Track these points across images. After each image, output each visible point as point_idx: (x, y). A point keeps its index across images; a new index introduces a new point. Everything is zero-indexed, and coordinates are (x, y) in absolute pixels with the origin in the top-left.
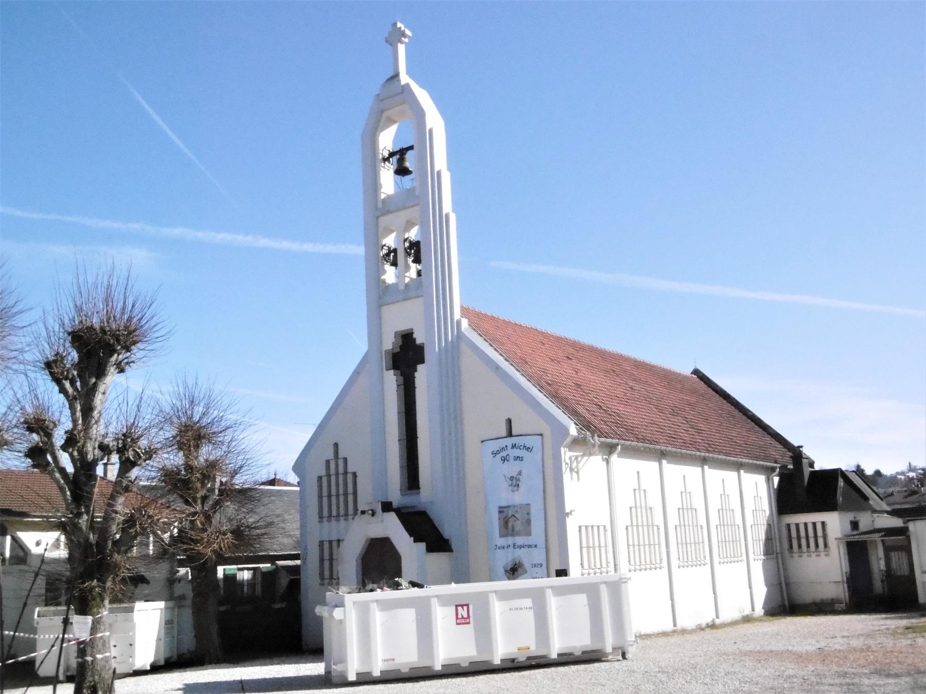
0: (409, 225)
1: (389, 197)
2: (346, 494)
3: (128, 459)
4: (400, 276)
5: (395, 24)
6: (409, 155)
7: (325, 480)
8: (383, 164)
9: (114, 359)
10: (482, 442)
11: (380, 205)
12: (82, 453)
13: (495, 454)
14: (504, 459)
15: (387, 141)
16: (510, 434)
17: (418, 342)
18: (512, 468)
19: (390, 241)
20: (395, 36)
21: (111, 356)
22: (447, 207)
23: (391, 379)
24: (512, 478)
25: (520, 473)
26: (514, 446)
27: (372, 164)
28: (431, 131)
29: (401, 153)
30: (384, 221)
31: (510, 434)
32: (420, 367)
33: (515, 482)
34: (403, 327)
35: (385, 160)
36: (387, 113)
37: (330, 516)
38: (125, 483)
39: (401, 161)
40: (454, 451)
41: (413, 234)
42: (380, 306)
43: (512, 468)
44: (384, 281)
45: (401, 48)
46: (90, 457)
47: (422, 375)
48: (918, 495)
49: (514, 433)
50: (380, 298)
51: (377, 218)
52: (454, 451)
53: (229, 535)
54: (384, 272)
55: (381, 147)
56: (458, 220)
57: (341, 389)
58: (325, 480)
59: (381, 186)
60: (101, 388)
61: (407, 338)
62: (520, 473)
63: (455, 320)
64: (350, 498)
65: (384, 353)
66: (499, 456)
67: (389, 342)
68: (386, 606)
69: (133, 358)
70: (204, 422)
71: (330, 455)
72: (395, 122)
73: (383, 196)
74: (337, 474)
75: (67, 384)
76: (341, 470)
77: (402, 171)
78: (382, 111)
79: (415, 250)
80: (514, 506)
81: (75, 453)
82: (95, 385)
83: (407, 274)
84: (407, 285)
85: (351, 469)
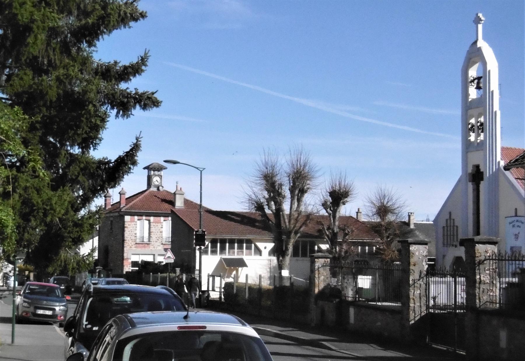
0: (479, 116)
1: (473, 100)
2: (453, 235)
3: (346, 233)
4: (476, 139)
5: (477, 14)
6: (482, 80)
7: (446, 228)
8: (470, 84)
9: (342, 201)
10: (506, 218)
11: (468, 104)
12: (333, 231)
13: (510, 223)
14: (514, 226)
15: (473, 73)
16: (516, 216)
17: (482, 170)
18: (516, 230)
19: (473, 121)
20: (478, 20)
21: (341, 200)
22: (496, 107)
23: (470, 186)
24: (516, 235)
25: (519, 233)
26: (517, 221)
27: (466, 83)
28: (489, 71)
29: (479, 78)
30: (470, 112)
31: (516, 216)
32: (482, 182)
33: (517, 236)
34: (476, 163)
35: (473, 81)
36: (473, 60)
37: (447, 244)
38: (345, 240)
39: (478, 83)
40: (455, 231)
41: (482, 119)
42: (467, 152)
43: (516, 230)
44: (470, 140)
45: (480, 26)
46: (335, 231)
47: (483, 185)
48: (165, 286)
49: (518, 214)
50: (467, 149)
51: (467, 110)
52: (455, 231)
53: (396, 252)
54: (470, 136)
55: (470, 76)
56: (502, 114)
57: (452, 188)
58: (446, 228)
59: (469, 95)
60: (338, 210)
61: (477, 167)
62: (519, 233)
63: (497, 161)
64: (455, 237)
65: (468, 174)
66: (511, 225)
67: (470, 170)
68: (436, 283)
69: (348, 200)
70: (389, 204)
71: (448, 217)
72: (478, 62)
73: (470, 100)
74: (450, 226)
75: (329, 210)
76: (452, 225)
77: (478, 88)
78: (470, 59)
79: (482, 127)
80: (516, 247)
81: (331, 231)
82: (337, 209)
83: (479, 138)
84: (478, 144)
85: (455, 225)
